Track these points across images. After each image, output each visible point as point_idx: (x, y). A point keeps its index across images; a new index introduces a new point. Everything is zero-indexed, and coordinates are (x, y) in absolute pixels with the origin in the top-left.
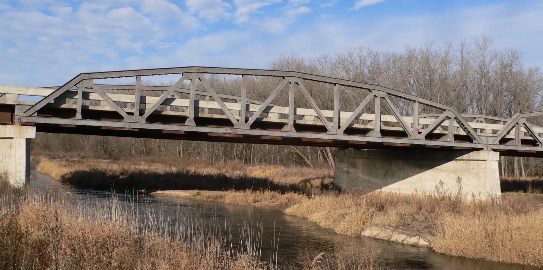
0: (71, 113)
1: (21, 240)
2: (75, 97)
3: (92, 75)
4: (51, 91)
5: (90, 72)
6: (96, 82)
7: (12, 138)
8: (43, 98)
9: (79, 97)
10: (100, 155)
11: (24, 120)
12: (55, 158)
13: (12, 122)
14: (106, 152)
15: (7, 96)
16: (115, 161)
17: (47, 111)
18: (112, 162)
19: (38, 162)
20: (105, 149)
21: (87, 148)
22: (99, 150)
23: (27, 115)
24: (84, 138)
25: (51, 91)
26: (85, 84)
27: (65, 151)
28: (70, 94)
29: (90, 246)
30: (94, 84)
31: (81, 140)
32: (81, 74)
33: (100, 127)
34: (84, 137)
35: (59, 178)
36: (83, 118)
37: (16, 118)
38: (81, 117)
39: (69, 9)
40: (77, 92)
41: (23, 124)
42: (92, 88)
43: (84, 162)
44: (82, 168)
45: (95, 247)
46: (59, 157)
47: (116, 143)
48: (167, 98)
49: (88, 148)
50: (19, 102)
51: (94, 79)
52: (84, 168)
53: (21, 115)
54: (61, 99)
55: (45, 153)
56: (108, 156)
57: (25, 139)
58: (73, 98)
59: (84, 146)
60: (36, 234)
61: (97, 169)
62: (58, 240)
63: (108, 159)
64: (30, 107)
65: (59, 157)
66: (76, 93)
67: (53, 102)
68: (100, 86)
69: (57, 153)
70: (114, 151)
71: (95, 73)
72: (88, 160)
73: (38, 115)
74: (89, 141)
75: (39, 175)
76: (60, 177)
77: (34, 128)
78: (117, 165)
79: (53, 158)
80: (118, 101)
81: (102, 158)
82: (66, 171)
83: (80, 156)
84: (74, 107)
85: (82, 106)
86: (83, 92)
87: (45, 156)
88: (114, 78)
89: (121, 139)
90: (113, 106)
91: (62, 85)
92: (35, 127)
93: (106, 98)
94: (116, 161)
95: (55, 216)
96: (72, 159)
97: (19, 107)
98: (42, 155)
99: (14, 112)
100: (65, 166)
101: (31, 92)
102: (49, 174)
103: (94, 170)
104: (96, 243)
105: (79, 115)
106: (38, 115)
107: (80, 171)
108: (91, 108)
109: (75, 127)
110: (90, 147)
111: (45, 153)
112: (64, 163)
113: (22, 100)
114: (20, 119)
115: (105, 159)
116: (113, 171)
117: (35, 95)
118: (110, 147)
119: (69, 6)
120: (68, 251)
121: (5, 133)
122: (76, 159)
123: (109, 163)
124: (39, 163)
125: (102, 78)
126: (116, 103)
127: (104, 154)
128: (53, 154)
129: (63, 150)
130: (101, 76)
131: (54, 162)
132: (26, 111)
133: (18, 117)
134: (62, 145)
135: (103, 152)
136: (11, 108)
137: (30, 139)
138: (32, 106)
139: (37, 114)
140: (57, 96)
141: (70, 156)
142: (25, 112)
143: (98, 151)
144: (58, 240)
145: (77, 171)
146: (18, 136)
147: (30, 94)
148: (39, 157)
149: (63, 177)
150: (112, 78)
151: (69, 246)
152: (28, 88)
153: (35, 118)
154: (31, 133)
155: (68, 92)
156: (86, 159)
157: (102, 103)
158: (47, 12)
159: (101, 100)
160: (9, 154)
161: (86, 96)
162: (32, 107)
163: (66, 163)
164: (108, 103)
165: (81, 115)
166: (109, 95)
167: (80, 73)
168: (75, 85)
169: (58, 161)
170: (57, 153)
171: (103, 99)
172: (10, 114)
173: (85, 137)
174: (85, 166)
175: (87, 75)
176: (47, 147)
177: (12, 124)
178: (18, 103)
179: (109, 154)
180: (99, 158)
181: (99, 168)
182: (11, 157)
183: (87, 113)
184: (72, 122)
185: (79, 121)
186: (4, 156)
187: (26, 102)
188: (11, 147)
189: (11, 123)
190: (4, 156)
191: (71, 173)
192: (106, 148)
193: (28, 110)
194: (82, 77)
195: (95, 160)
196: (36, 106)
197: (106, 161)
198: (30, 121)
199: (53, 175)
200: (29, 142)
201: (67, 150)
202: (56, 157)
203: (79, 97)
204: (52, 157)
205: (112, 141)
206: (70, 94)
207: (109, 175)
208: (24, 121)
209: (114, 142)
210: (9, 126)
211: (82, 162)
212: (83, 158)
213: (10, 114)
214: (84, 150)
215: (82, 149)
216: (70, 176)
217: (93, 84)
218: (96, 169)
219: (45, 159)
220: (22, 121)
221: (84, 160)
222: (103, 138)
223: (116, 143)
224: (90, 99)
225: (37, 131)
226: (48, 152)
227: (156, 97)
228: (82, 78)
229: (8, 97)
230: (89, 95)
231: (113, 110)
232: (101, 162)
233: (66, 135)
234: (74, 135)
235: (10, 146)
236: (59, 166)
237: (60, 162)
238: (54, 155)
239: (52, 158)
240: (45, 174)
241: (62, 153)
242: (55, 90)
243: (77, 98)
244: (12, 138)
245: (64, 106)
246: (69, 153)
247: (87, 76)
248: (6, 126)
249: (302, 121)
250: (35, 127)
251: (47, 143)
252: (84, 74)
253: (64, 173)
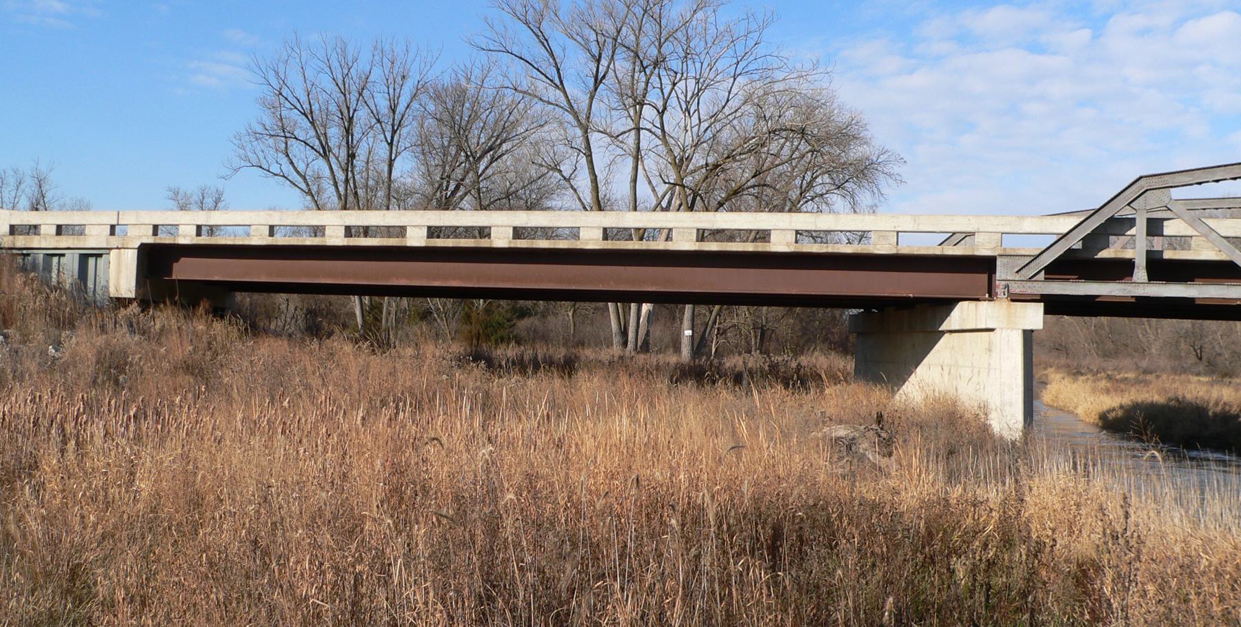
0: (1122, 269)
1: (1039, 557)
2: (1129, 233)
3: (1166, 178)
4: (1073, 221)
5: (1163, 172)
6: (1176, 193)
7: (992, 330)
8: (1055, 238)
9: (1139, 230)
10: (1185, 366)
11: (1016, 289)
12: (1082, 374)
13: (991, 294)
14: (1200, 359)
15: (978, 238)
16: (1225, 380)
17: (1066, 266)
18: (1217, 382)
19: (1044, 383)
20: (1199, 351)
21: (1153, 351)
22: (1183, 354)
23: (1023, 279)
24: (1147, 328)
25: (1074, 221)
26: (1153, 199)
27: (1104, 357)
28: (1117, 225)
29: (1204, 580)
30: (1174, 198)
31: (1139, 331)
32: (1141, 178)
33: (1192, 300)
34: (1146, 323)
35: (1093, 418)
36: (1150, 279)
37: (998, 287)
38: (1146, 277)
39: (1084, 35)
40: (1134, 219)
41: (1016, 299)
42: (1169, 209)
43: (1150, 382)
44: (1147, 396)
45: (1215, 584)
46: (1091, 371)
47: (1225, 337)
48: (1135, 226)
49: (1156, 350)
50: (1005, 249)
51: (1171, 187)
52: (1152, 394)
53: (1009, 278)
54: (1099, 237)
55: (1056, 362)
56: (1207, 368)
57: (1020, 334)
58: (1124, 235)
59: (1147, 344)
60: (1086, 544)
61: (1184, 397)
62: (1130, 563)
63: (1205, 374)
64: (1028, 260)
65: (1091, 371)
66: (1131, 222)
67: (1079, 246)
68: (1186, 204)
69: (1086, 362)
70: (1220, 355)
71: (1175, 173)
72: (1158, 377)
73: (1047, 276)
74: (1157, 334)
75: (1052, 414)
76: (1097, 417)
77: (1040, 307)
78: (1231, 390)
79: (1076, 372)
80: (1234, 235)
81: (1192, 373)
82: (1111, 402)
83: (1138, 368)
84: (1128, 254)
85: (1148, 252)
86: (1149, 220)
87: (1059, 368)
88: (1203, 185)
89: (1236, 326)
90: (1222, 249)
91: (1098, 207)
92: (1042, 304)
93: (1203, 229)
94: (1227, 380)
95: (1122, 507)
96: (1121, 375)
97: (1005, 260)
98: (1051, 367)
99: (995, 273)
100: (1107, 391)
101: (1029, 225)
102: (1071, 408)
103: (1177, 400)
104: (1219, 575)
105: (1140, 274)
106: (1047, 276)
107: (1142, 403)
108: (1168, 255)
109: (1133, 300)
110: (1161, 347)
111: (1056, 362)
112: (1103, 384)
113: (1011, 245)
114: (1007, 286)
115: (1198, 374)
116: (1222, 402)
117: (1039, 232)
118: (1210, 346)
119: (1083, 27)
120: (1151, 588)
121: (976, 319)
122: (1131, 375)
123: (1212, 384)
124: (1046, 384)
125: (1192, 184)
126: (1229, 242)
127: (1197, 363)
128: (1075, 364)
129: (1097, 354)
130: (1190, 179)
131: (1080, 382)
132: (1020, 270)
133: (1003, 283)
134: (1096, 342)
135: (1192, 359)
136: (986, 265)
137: (1032, 331)
138: (1033, 258)
139: (1045, 274)
140: (1089, 232)
141: (1115, 369)
142: (1017, 272)
143: (1181, 357)
144: (1130, 563)
145: (1137, 403)
146: (1004, 326)
147: (1028, 231)
148: (1045, 372)
149: (1103, 417)
150: (1217, 181)
151: (1153, 578)
152: (1021, 217)
153: (1040, 284)
154: (1034, 316)
155: (1112, 220)
156: (1154, 375)
157: (1193, 242)
158: (1036, 48)
159: (1191, 237)
160: (987, 366)
161: (1155, 227)
162: (1033, 260)
163: (1108, 385)
164: (1209, 241)
165: (1146, 274)
166: (1211, 222)
167: (1138, 176)
168: (1129, 204)
169: (1088, 379)
170: (1086, 362)
171: (1195, 233)
172: (985, 276)
173: (1150, 325)
174: (1154, 391)
175: (1155, 179)
176: (1060, 348)
177: (991, 298)
178: (1001, 253)
179: (1208, 362)
180: (1185, 372)
181: (1189, 397)
182: (992, 372)
183: (1160, 269)
184: (1125, 290)
185: (1141, 286)
186: (976, 370)
187: (1018, 249)
188: (990, 350)
189: (990, 296)
190: (976, 370)
191: (1121, 407)
192: (1201, 348)
193: (1024, 267)
194: (1142, 186)
195: (1177, 378)
196: (1042, 257)
197: (1201, 379)
198: (1029, 291)
199: (1080, 411)
200: (1028, 336)
201: (1106, 355)
202: (1083, 371)
203: (1139, 230)
204: (1074, 371)
205: (1214, 332)
206: (1117, 225)
207: (1213, 413)
208: (1018, 291)
209: (1219, 334)
210: (985, 304)
211: (1147, 383)
212: (1146, 372)
213: (985, 276)
214: (1146, 353)
215: (1143, 351)
216: (1120, 413)
217: (1171, 199)
218: (1181, 399)
219: (1059, 376)
220: (1012, 291)
221: (1149, 377)
222: (1193, 325)
223: (1225, 337)
224: (1165, 234)
225: (1047, 312)
226: (1063, 361)
227: (366, 224)
228: (1143, 188)
229: (980, 240)
230: (1163, 226)
231: (1223, 257)
232: (1189, 382)
233: (1104, 319)
234: (1121, 319)
235: (987, 347)
236: (1094, 391)
237: (1094, 381)
238: (1079, 366)
239: (1074, 374)
240: (1061, 410)
241: (1095, 362)
242: (1082, 219)
243: (1134, 233)
244: (992, 330)
245: (1104, 254)
246: (1112, 363)
247: (1155, 183)
248: (978, 303)
249: (1137, 262)
250: (1042, 304)
251: (1060, 338)
252: (1148, 176)
253: (1105, 408)
